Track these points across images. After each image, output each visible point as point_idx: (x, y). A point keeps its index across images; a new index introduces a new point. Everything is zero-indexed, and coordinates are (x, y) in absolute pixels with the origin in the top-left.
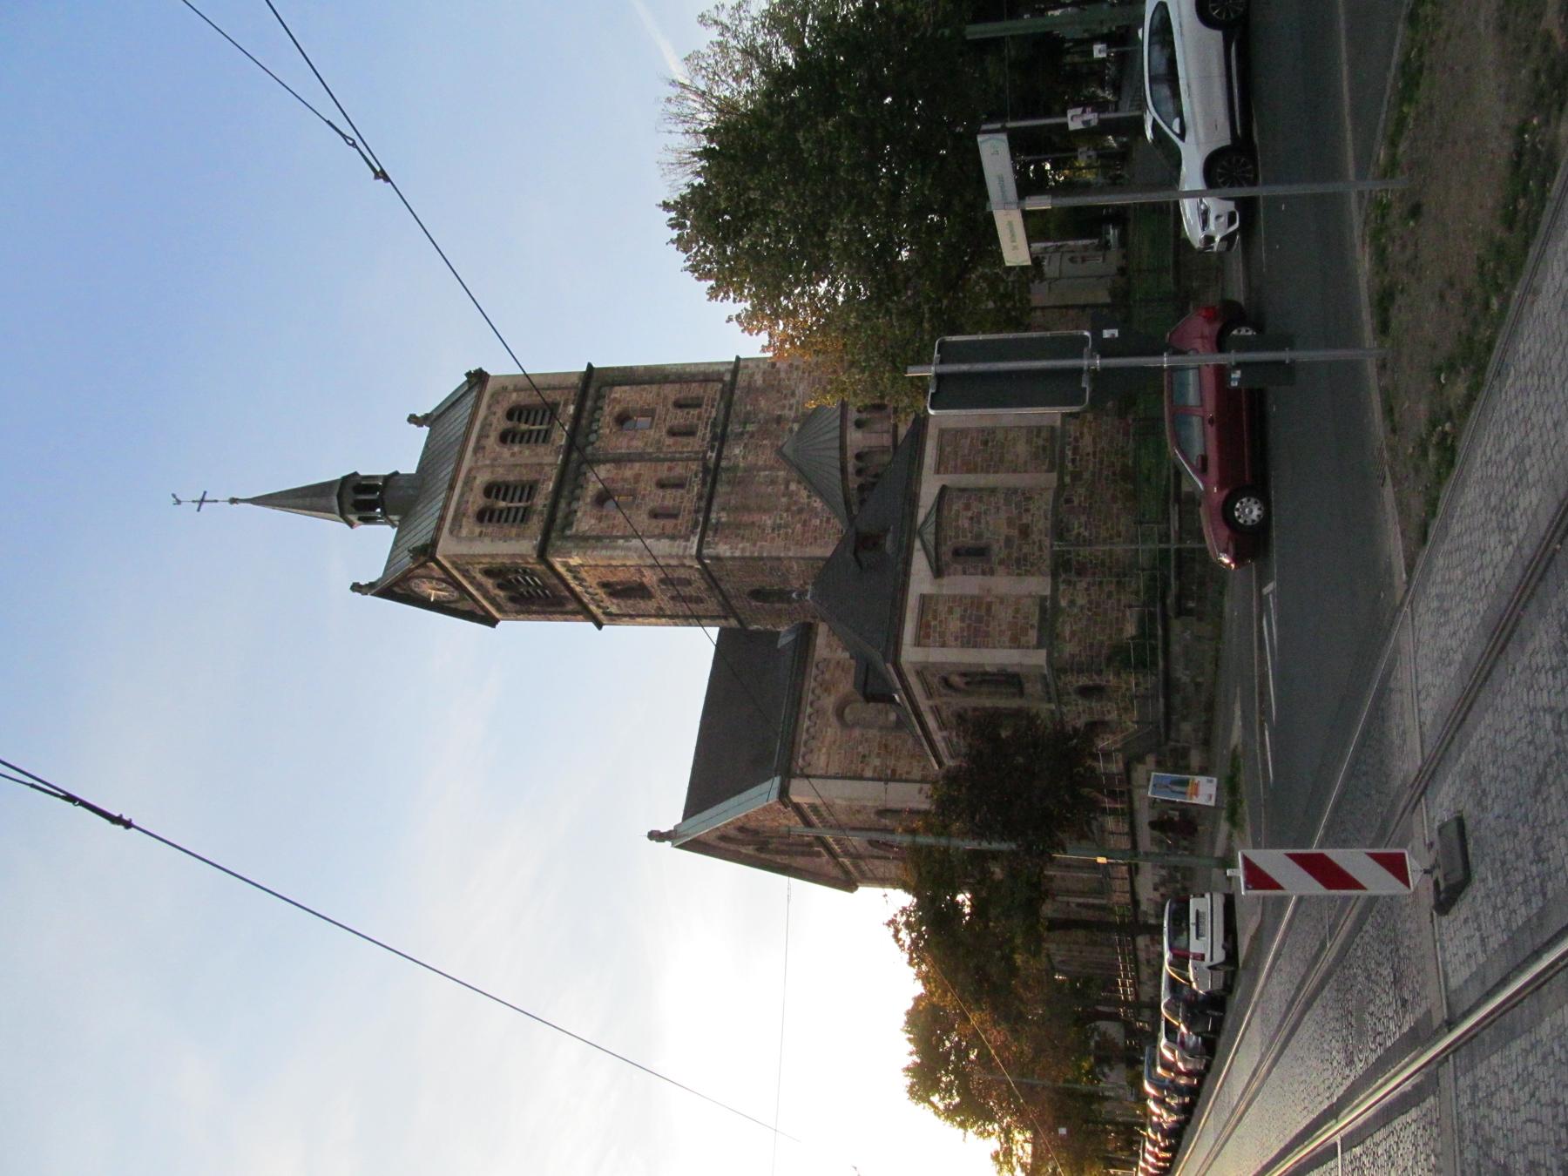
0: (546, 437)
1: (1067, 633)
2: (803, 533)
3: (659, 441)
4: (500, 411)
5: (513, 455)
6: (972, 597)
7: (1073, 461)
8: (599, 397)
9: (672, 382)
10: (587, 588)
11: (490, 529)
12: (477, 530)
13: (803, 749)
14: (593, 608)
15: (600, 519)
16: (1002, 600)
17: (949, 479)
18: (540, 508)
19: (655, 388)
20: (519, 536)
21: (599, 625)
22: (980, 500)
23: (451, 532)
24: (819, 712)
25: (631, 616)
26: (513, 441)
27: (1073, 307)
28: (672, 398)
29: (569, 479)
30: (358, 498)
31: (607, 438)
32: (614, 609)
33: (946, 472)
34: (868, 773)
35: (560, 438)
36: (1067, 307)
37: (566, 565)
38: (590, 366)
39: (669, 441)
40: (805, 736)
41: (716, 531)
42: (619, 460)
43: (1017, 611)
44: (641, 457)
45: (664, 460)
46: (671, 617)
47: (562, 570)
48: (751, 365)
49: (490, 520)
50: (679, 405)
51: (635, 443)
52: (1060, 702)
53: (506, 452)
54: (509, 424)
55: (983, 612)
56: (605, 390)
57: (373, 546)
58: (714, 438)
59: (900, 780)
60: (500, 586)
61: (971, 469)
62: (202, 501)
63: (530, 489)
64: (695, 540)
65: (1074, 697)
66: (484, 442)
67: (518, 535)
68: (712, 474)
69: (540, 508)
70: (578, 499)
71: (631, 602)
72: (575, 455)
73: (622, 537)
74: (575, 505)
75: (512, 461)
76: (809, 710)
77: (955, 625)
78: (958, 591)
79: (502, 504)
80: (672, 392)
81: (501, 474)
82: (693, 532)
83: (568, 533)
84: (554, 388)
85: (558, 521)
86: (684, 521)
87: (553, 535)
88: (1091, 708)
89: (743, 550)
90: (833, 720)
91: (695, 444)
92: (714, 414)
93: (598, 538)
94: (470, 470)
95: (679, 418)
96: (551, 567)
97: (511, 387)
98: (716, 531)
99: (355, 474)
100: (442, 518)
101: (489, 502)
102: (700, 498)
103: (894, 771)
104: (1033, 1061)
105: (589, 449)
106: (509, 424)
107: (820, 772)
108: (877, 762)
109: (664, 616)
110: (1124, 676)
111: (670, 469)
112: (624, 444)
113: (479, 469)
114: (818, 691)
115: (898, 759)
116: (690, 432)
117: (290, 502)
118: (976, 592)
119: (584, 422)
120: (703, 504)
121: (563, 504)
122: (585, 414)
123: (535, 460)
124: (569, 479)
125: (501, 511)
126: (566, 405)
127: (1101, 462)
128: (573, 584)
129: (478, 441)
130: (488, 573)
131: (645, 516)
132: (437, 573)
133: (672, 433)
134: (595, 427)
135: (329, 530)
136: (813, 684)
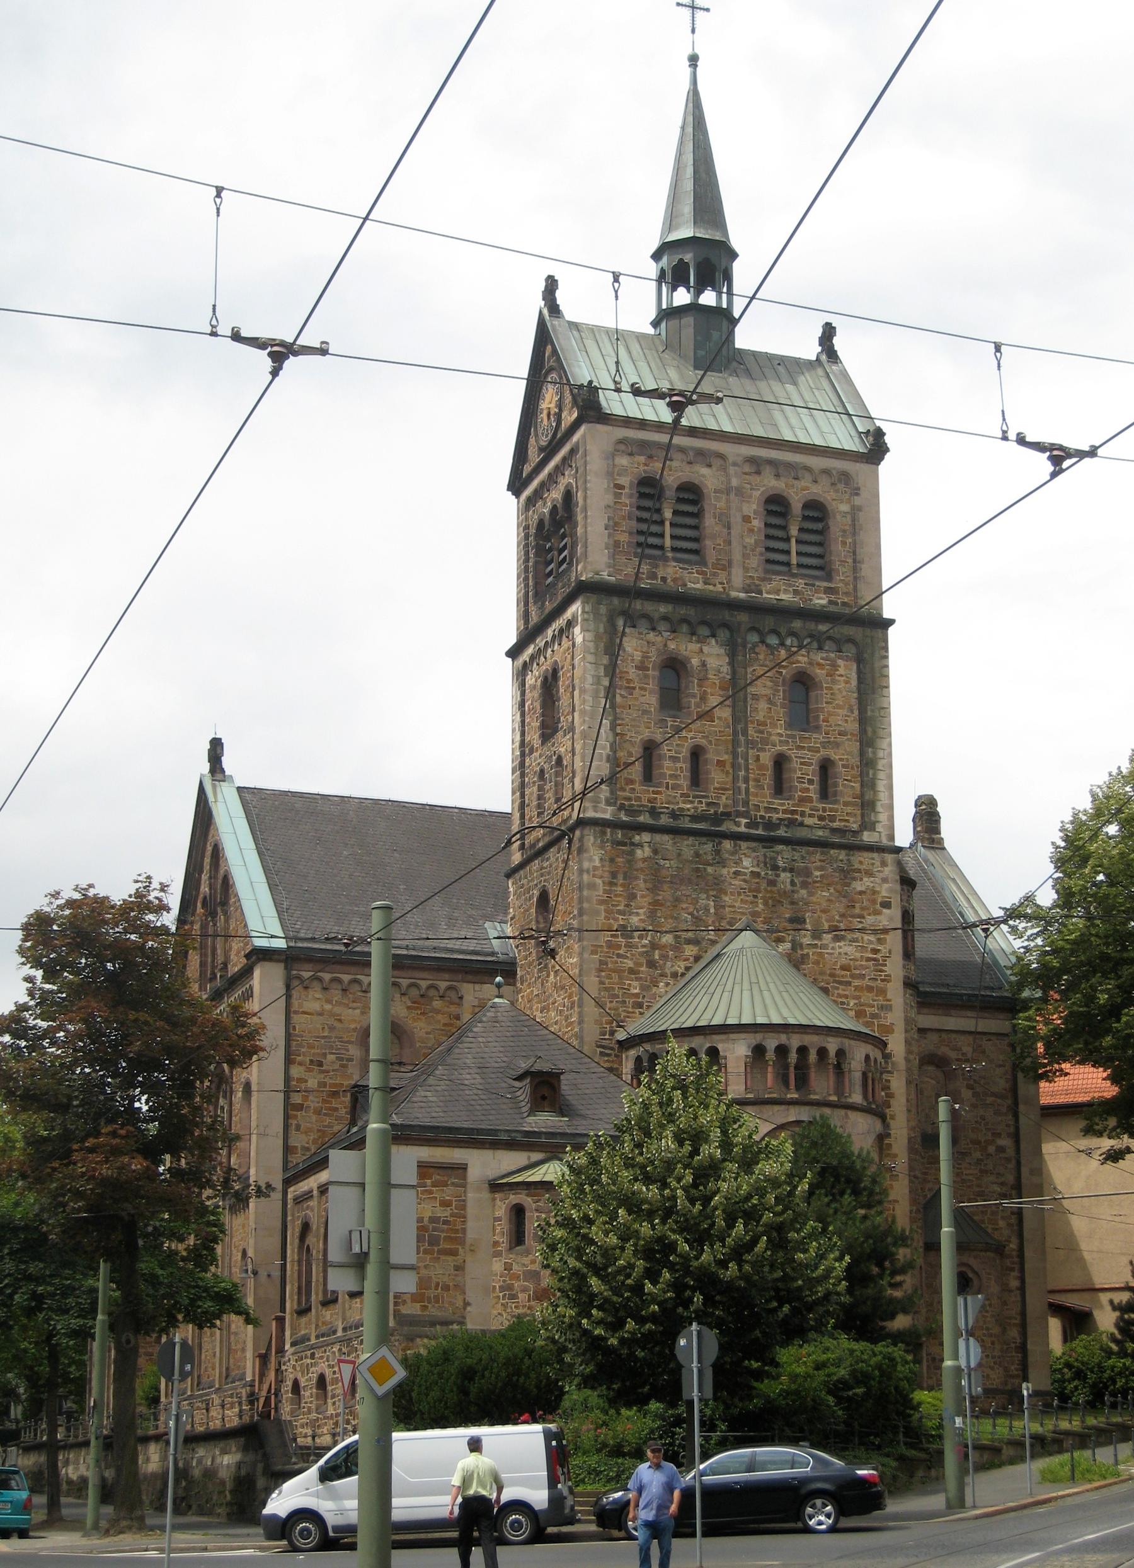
2: (619, 971)
3: (765, 741)
4: (820, 490)
5: (746, 519)
6: (464, 1231)
8: (839, 644)
9: (862, 753)
11: (628, 500)
12: (624, 481)
14: (530, 650)
15: (642, 667)
16: (460, 1268)
18: (660, 573)
19: (854, 727)
20: (616, 547)
21: (513, 653)
23: (620, 442)
25: (522, 704)
28: (834, 756)
29: (708, 614)
30: (698, 258)
32: (530, 680)
34: (296, 1071)
35: (780, 592)
38: (891, 622)
39: (766, 758)
40: (346, 978)
42: (736, 690)
43: (446, 1288)
44: (740, 718)
45: (735, 754)
46: (522, 765)
47: (569, 614)
49: (642, 495)
50: (825, 767)
51: (763, 705)
53: (753, 507)
54: (797, 507)
57: (616, 299)
58: (769, 825)
59: (287, 1117)
63: (691, 549)
64: (607, 813)
66: (768, 471)
68: (711, 829)
69: (660, 573)
71: (538, 705)
74: (663, 626)
75: (736, 520)
78: (471, 1211)
79: (668, 514)
80: (845, 754)
81: (714, 504)
83: (620, 622)
84: (855, 569)
86: (643, 794)
87: (616, 601)
89: (591, 886)
91: (762, 798)
92: (808, 821)
93: (612, 670)
94: (721, 456)
95: (804, 771)
97: (857, 501)
99: (733, 255)
101: (670, 493)
102: (674, 815)
103: (300, 1107)
104: (994, 1095)
105: (753, 638)
106: (797, 507)
107: (295, 1003)
108: (312, 1083)
109: (523, 754)
111: (721, 764)
114: (414, 992)
115: (318, 1112)
116: (779, 788)
117: (689, 158)
118: (471, 1235)
119: (797, 624)
120: (664, 820)
121: (664, 609)
122: (811, 625)
123: (737, 556)
124: (708, 614)
126: (829, 591)
129: (770, 462)
130: (568, 496)
131: (646, 734)
133: (780, 762)
135: (644, 219)
136: (424, 984)
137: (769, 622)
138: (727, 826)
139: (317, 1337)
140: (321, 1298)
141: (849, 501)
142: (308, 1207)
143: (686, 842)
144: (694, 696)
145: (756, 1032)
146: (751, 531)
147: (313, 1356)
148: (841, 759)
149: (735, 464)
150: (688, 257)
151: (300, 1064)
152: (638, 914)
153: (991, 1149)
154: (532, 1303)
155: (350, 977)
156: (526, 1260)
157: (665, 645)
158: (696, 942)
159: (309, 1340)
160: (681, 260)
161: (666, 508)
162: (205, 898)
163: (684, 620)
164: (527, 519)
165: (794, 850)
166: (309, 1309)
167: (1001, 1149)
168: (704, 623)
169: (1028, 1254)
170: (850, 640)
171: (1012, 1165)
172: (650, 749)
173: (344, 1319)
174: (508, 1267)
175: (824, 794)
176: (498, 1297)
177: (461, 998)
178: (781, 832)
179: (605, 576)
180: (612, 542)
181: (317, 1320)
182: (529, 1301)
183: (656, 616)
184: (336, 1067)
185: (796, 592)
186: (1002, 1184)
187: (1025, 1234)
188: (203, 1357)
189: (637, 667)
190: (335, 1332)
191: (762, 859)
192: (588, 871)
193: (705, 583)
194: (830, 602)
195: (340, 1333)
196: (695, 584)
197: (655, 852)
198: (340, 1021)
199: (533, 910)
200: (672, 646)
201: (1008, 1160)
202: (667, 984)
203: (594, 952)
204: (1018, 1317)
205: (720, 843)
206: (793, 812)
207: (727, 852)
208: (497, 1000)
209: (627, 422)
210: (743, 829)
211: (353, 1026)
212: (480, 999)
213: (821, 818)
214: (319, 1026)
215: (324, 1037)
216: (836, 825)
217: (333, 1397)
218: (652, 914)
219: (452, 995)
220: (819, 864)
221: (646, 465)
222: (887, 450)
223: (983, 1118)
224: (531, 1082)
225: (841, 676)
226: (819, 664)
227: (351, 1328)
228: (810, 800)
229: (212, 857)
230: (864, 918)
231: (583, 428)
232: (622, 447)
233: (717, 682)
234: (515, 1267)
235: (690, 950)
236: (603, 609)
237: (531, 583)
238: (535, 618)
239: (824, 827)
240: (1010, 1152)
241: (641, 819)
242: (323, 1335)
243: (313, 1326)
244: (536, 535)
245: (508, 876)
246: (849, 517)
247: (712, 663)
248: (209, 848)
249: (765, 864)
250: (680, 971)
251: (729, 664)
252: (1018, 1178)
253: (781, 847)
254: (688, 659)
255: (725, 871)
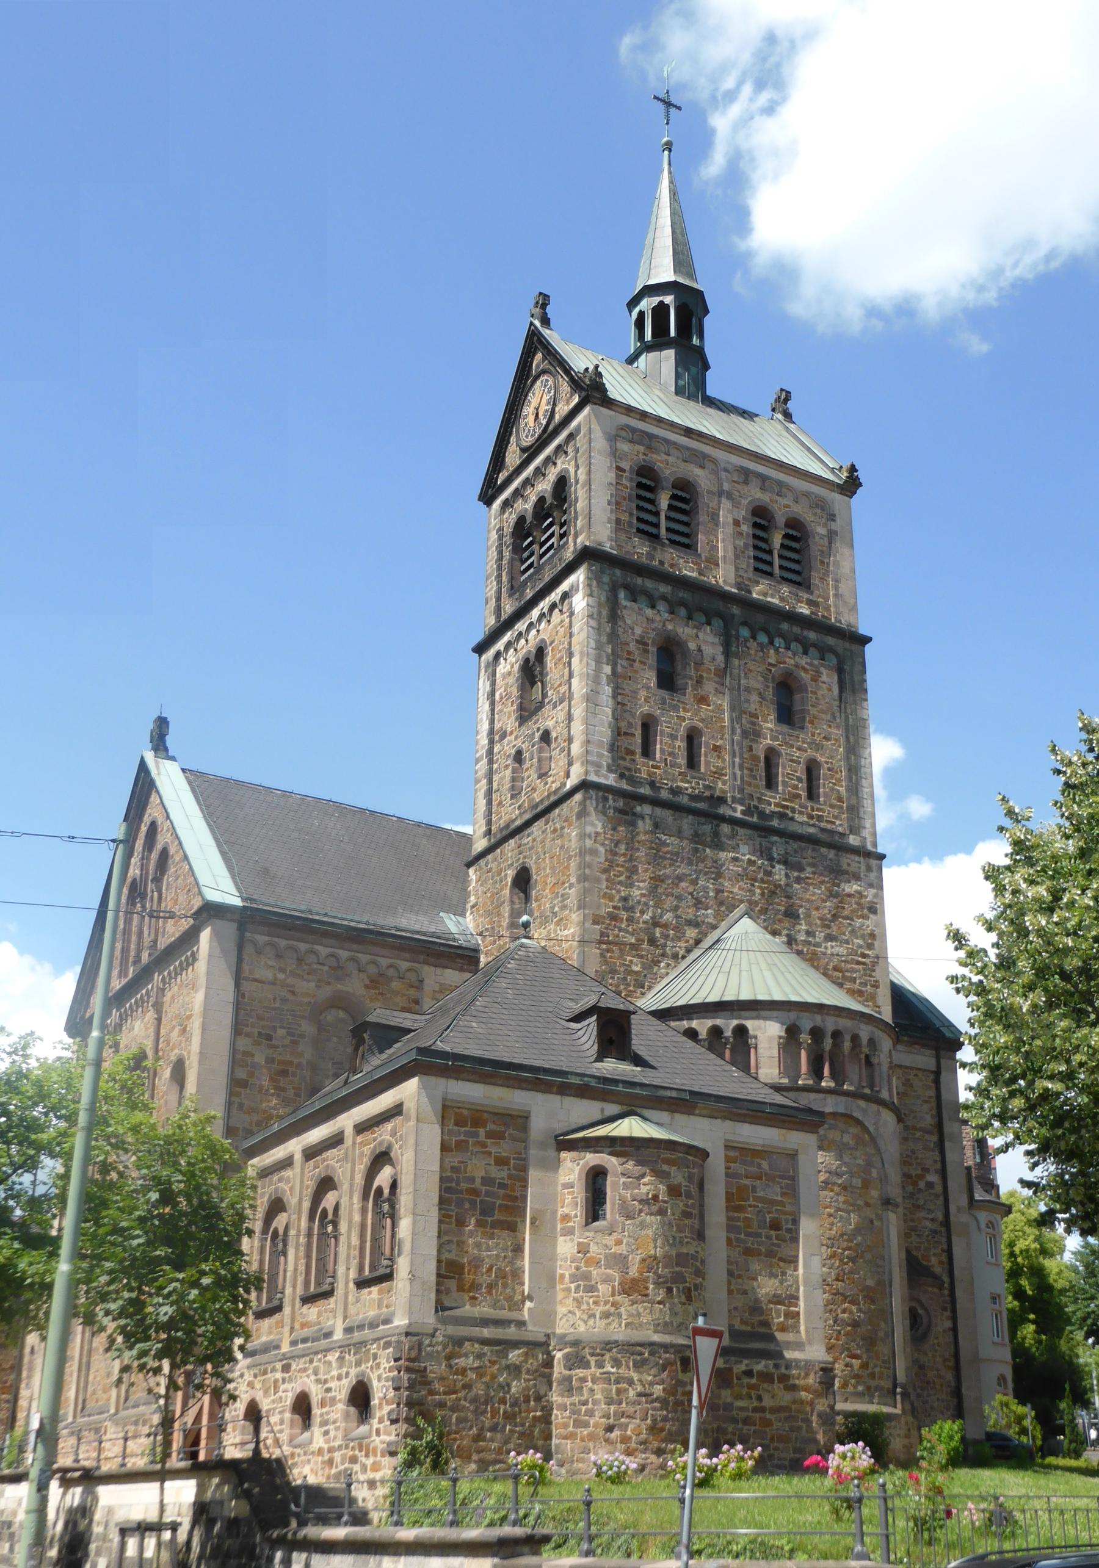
0: (763, 568)
1: (461, 1362)
4: (801, 510)
7: (749, 1373)
8: (823, 651)
10: (540, 629)
12: (625, 465)
13: (283, 943)
15: (641, 642)
17: (717, 1163)
22: (686, 1215)
24: (338, 971)
26: (755, 525)
27: (958, 1377)
31: (760, 663)
33: (728, 1159)
36: (957, 1368)
37: (574, 589)
38: (866, 640)
40: (303, 947)
41: (622, 812)
47: (565, 586)
48: (873, 875)
49: (640, 485)
50: (812, 770)
51: (754, 697)
52: (344, 1347)
55: (498, 1216)
56: (833, 660)
60: (541, 500)
61: (735, 1200)
62: (668, 104)
63: (685, 542)
65: (353, 1372)
66: (754, 482)
67: (618, 521)
70: (672, 612)
72: (735, 610)
73: (614, 672)
74: (662, 606)
76: (344, 954)
77: (478, 1168)
82: (622, 776)
83: (622, 594)
85: (639, 581)
88: (333, 1402)
90: (326, 992)
93: (613, 637)
94: (714, 461)
96: (570, 569)
97: (834, 526)
98: (622, 812)
100: (644, 415)
106: (780, 519)
107: (246, 967)
110: (387, 1461)
112: (753, 683)
113: (716, 473)
119: (785, 626)
120: (664, 795)
121: (664, 589)
122: (796, 630)
124: (702, 601)
125: (652, 502)
126: (811, 603)
127: (746, 1421)
128: (544, 604)
130: (562, 482)
132: (562, 410)
134: (778, 642)
137: (760, 618)
138: (723, 810)
139: (294, 1343)
140: (300, 1291)
141: (825, 525)
142: (280, 1180)
143: (685, 821)
144: (691, 678)
145: (789, 1011)
146: (741, 534)
147: (286, 1368)
148: (827, 763)
149: (726, 470)
150: (669, 299)
151: (247, 1035)
152: (639, 888)
153: (922, 1185)
154: (618, 1298)
155: (307, 946)
156: (610, 1240)
157: (664, 625)
158: (696, 924)
159: (278, 1347)
160: (661, 302)
161: (662, 495)
162: (134, 880)
163: (683, 603)
164: (501, 521)
165: (787, 843)
166: (279, 1309)
167: (930, 1185)
168: (701, 609)
169: (959, 1293)
170: (832, 650)
171: (940, 1201)
172: (648, 726)
173: (345, 1318)
174: (583, 1249)
175: (812, 795)
176: (569, 1290)
177: (422, 981)
178: (775, 823)
179: (608, 547)
180: (614, 518)
181: (293, 1319)
182: (613, 1295)
183: (656, 594)
184: (287, 1041)
185: (782, 599)
186: (933, 1220)
187: (956, 1273)
188: (91, 1378)
189: (638, 642)
190: (328, 1335)
191: (758, 847)
192: (590, 836)
193: (700, 574)
194: (812, 613)
195: (338, 1335)
196: (689, 571)
197: (656, 825)
198: (293, 993)
199: (507, 892)
200: (670, 627)
201: (937, 1196)
202: (668, 965)
203: (595, 922)
204: (952, 1359)
205: (718, 826)
206: (786, 807)
207: (725, 835)
208: (524, 940)
209: (629, 410)
210: (738, 815)
211: (306, 1000)
212: (441, 984)
213: (811, 817)
214: (271, 996)
215: (275, 1009)
216: (823, 825)
217: (325, 1423)
218: (653, 891)
219: (412, 976)
220: (810, 860)
221: (644, 454)
222: (860, 485)
223: (913, 1152)
224: (598, 1019)
225: (824, 682)
226: (804, 669)
227: (361, 1327)
228: (799, 796)
229: (147, 836)
230: (852, 920)
231: (587, 410)
232: (623, 434)
233: (713, 668)
234: (594, 1249)
235: (691, 933)
236: (606, 579)
237: (504, 579)
238: (509, 608)
239: (814, 825)
240: (939, 1189)
241: (642, 791)
242: (304, 1340)
243: (287, 1329)
244: (513, 534)
245: (469, 865)
246: (826, 539)
247: (708, 650)
248: (144, 829)
249: (761, 853)
250: (681, 953)
251: (723, 653)
252: (947, 1215)
253: (775, 838)
254: (686, 642)
255: (723, 855)
